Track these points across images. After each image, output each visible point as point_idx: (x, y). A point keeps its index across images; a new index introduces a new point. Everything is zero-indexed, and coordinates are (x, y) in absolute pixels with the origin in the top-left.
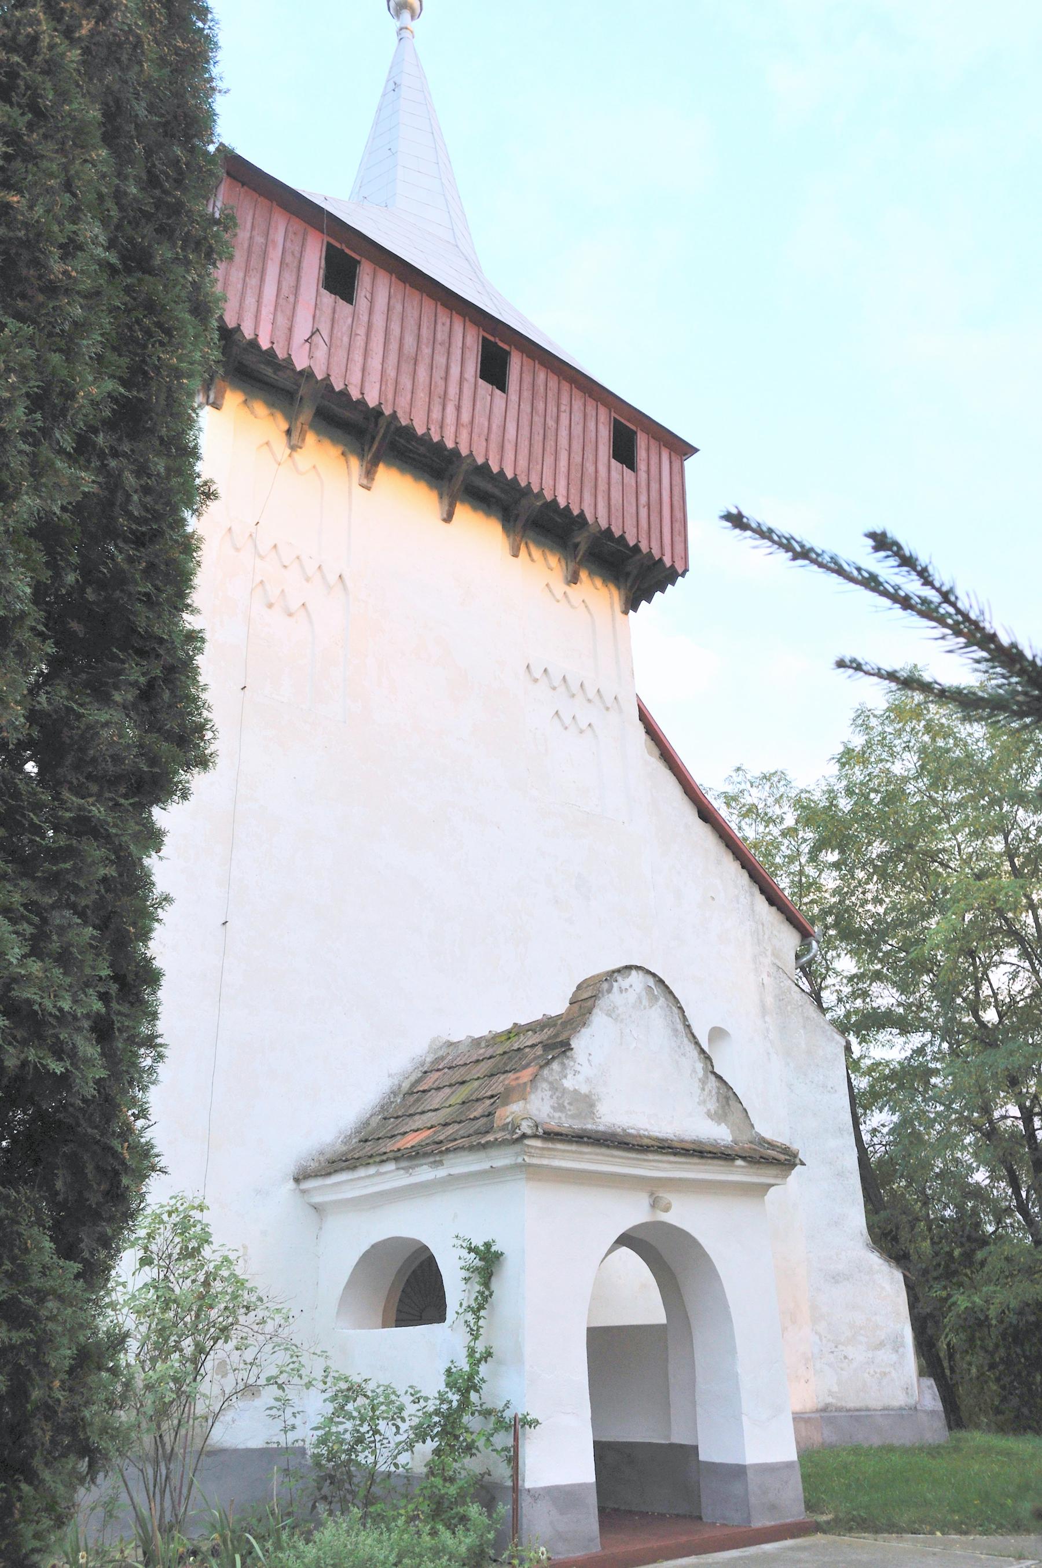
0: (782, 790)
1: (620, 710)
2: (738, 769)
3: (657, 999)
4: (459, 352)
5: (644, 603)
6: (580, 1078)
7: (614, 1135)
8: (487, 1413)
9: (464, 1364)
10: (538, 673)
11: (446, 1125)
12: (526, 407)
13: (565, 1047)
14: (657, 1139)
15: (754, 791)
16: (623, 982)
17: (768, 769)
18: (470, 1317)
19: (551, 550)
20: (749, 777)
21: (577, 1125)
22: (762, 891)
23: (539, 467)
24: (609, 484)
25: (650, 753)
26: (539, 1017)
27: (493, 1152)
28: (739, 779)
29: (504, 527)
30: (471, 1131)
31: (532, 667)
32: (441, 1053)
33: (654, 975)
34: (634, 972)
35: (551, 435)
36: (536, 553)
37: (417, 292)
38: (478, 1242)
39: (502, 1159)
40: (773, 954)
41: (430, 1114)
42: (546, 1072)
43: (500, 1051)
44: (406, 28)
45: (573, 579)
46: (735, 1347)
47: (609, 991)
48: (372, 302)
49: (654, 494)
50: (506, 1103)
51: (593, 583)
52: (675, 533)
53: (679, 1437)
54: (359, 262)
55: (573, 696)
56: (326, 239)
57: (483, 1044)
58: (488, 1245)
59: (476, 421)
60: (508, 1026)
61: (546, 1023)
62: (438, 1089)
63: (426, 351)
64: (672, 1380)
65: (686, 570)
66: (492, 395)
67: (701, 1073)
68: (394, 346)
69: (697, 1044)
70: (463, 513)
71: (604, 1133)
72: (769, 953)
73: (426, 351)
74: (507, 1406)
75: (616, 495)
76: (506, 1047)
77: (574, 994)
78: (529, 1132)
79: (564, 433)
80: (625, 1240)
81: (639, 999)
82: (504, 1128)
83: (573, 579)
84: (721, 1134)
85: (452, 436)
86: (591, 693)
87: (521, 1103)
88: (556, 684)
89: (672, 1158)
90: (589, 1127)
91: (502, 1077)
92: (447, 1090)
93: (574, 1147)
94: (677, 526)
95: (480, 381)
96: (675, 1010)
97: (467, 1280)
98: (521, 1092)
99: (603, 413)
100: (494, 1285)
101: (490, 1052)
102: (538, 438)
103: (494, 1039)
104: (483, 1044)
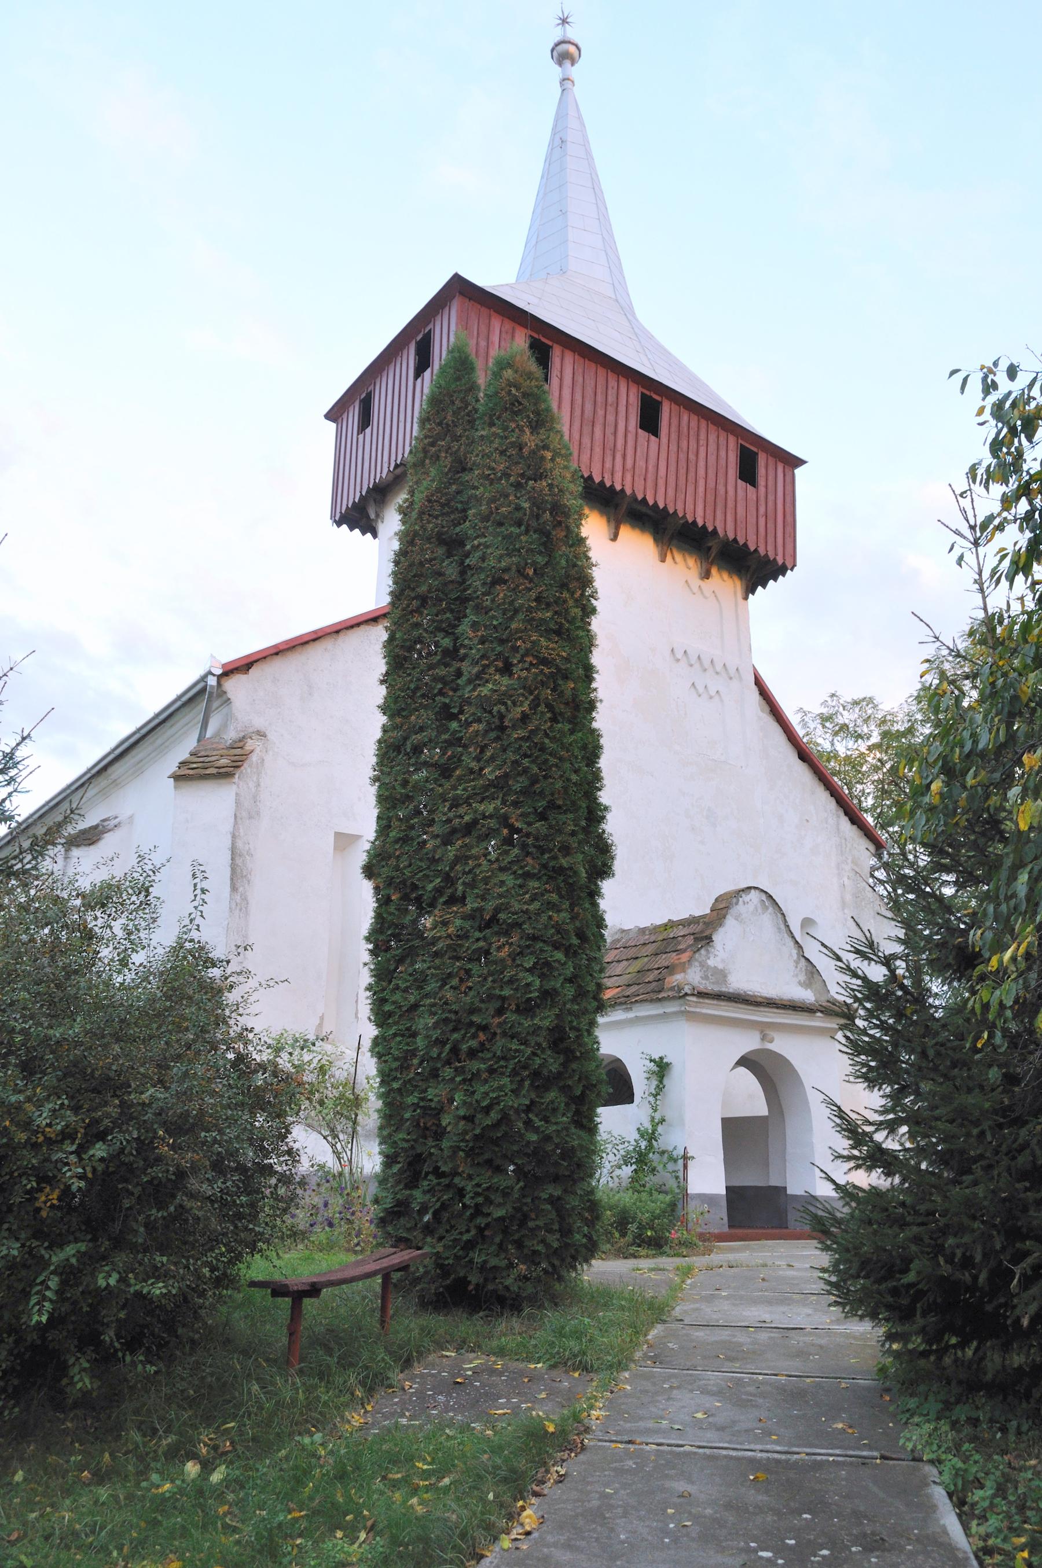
0: (870, 712)
1: (741, 679)
2: (833, 695)
3: (767, 908)
4: (624, 408)
5: (760, 588)
6: (718, 959)
7: (739, 995)
8: (663, 1152)
9: (648, 1125)
10: (679, 655)
11: (629, 985)
12: (673, 447)
13: (709, 939)
14: (766, 998)
15: (845, 713)
16: (746, 898)
17: (858, 696)
18: (652, 1099)
19: (690, 553)
20: (841, 701)
21: (716, 988)
22: (846, 814)
23: (683, 496)
24: (736, 501)
25: (762, 710)
26: (687, 916)
27: (666, 1003)
28: (834, 704)
29: (656, 540)
30: (649, 990)
31: (675, 650)
32: (616, 937)
33: (766, 893)
34: (753, 891)
35: (692, 469)
36: (678, 557)
37: (593, 365)
38: (656, 1057)
39: (671, 1008)
40: (853, 862)
41: (616, 978)
42: (697, 955)
43: (661, 938)
44: (568, 79)
45: (706, 575)
46: (811, 1127)
47: (737, 904)
48: (561, 380)
49: (770, 504)
50: (672, 974)
51: (721, 576)
52: (787, 536)
53: (774, 1182)
54: (552, 347)
55: (705, 670)
56: (530, 332)
57: (647, 932)
58: (661, 1058)
59: (637, 464)
60: (665, 921)
61: (692, 921)
62: (619, 961)
63: (600, 412)
64: (770, 1150)
65: (795, 565)
66: (648, 441)
67: (795, 957)
68: (578, 412)
69: (793, 937)
70: (626, 533)
71: (733, 994)
72: (849, 861)
73: (600, 412)
74: (675, 1148)
75: (741, 511)
76: (664, 935)
77: (714, 904)
78: (689, 992)
79: (702, 464)
80: (744, 1062)
81: (756, 908)
82: (672, 989)
83: (706, 575)
84: (807, 996)
85: (620, 480)
86: (719, 667)
87: (682, 975)
88: (693, 662)
89: (775, 1010)
90: (724, 989)
91: (664, 956)
92: (625, 963)
93: (715, 1002)
94: (789, 529)
95: (640, 431)
96: (779, 915)
97: (648, 1079)
98: (683, 968)
99: (732, 439)
100: (665, 1081)
101: (653, 938)
102: (682, 472)
103: (655, 929)
104: (647, 932)
